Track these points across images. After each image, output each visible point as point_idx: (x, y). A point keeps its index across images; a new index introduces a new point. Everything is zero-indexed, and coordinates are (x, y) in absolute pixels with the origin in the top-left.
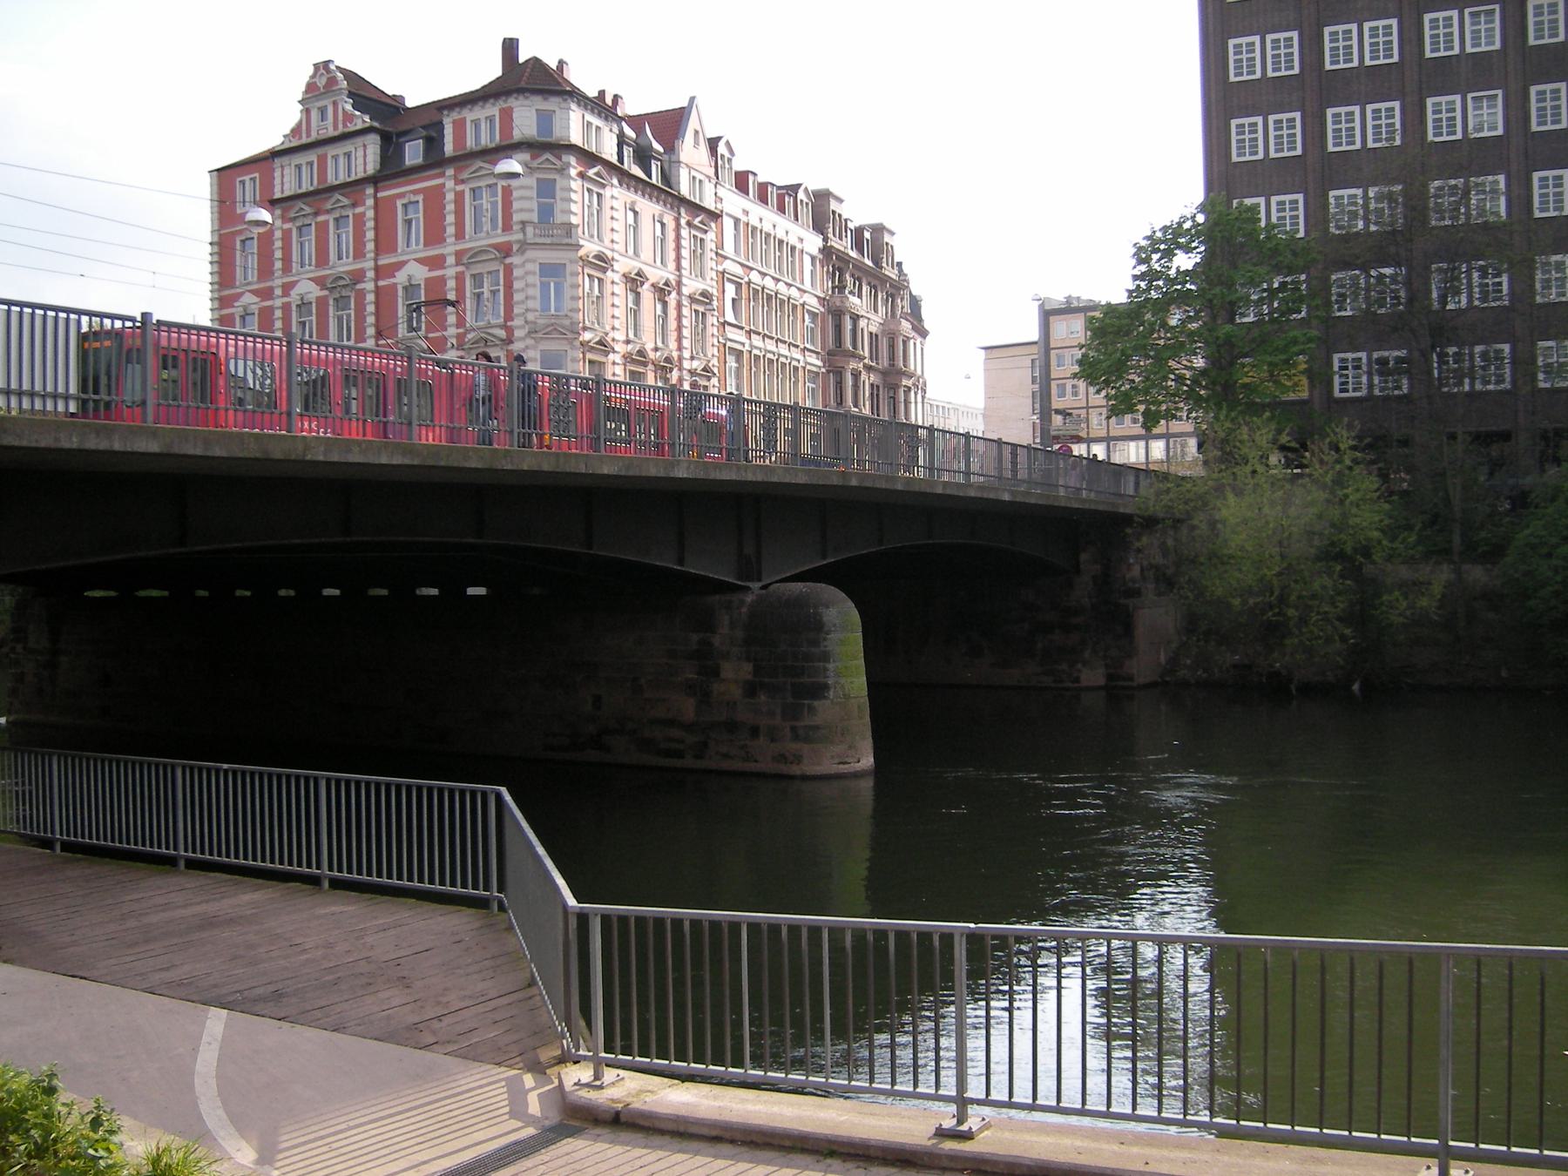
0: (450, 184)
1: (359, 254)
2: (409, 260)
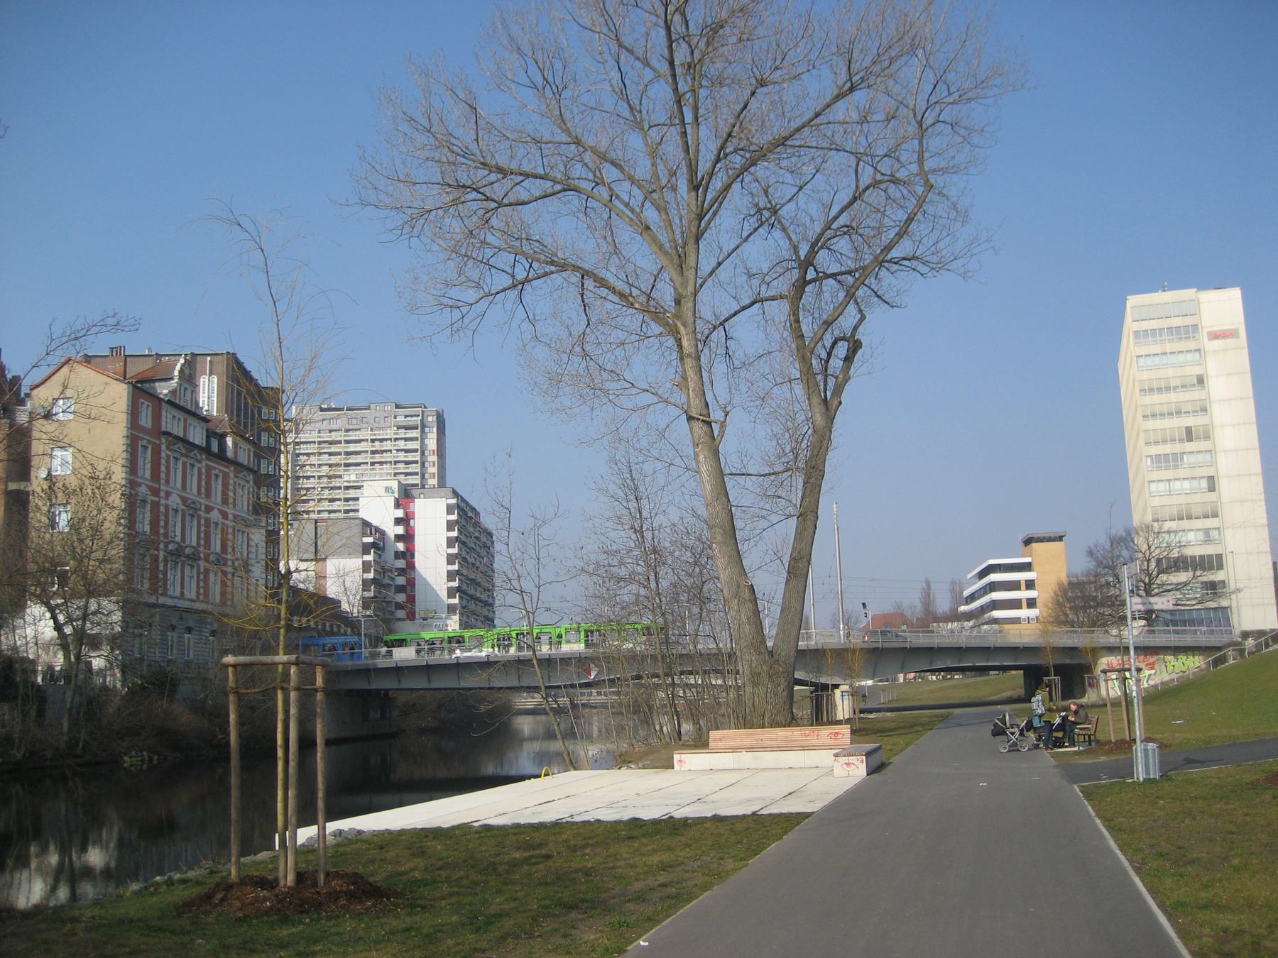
0: (232, 475)
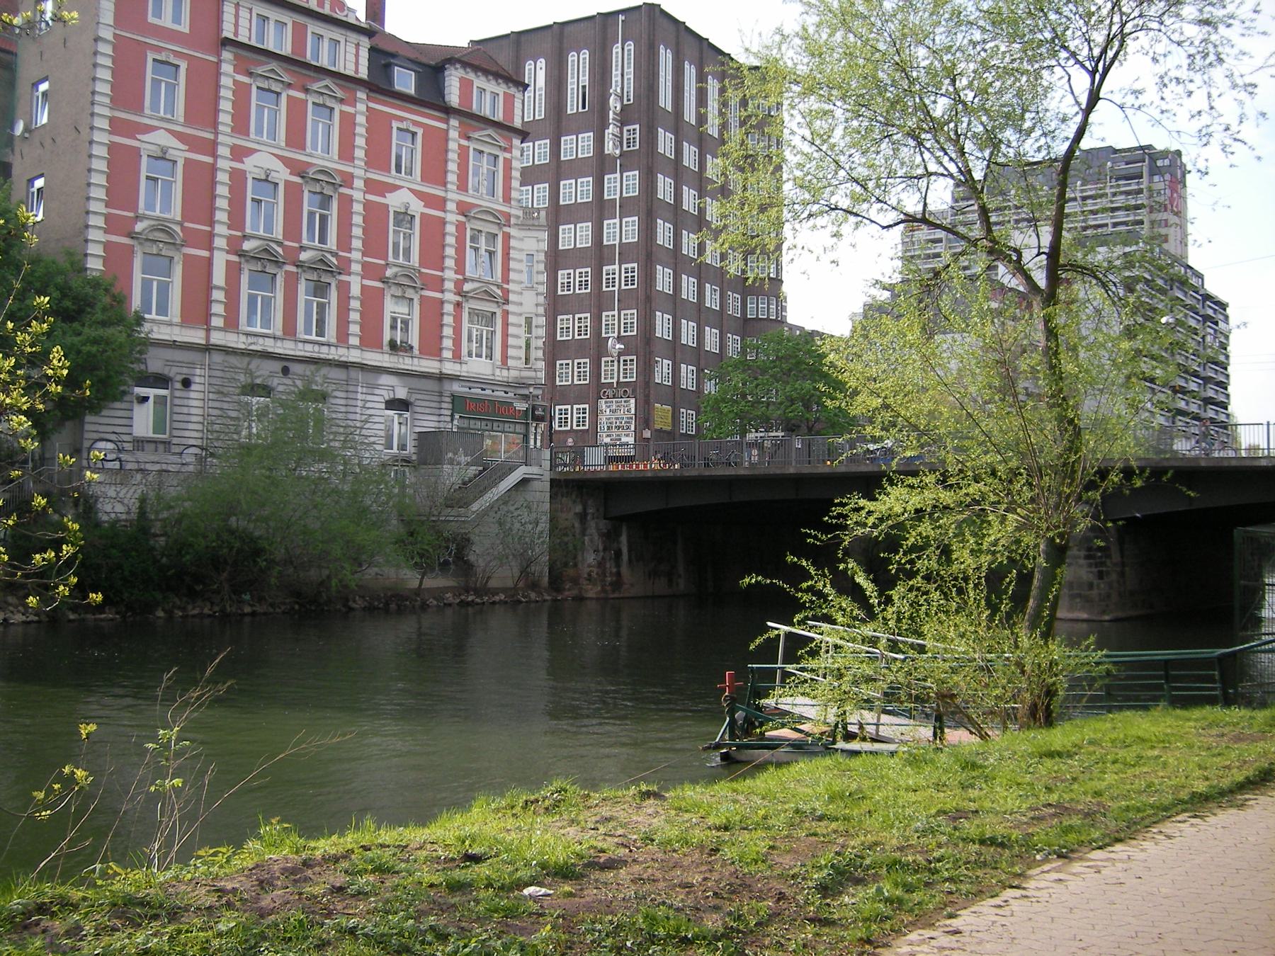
0: (453, 134)
1: (346, 153)
2: (400, 187)
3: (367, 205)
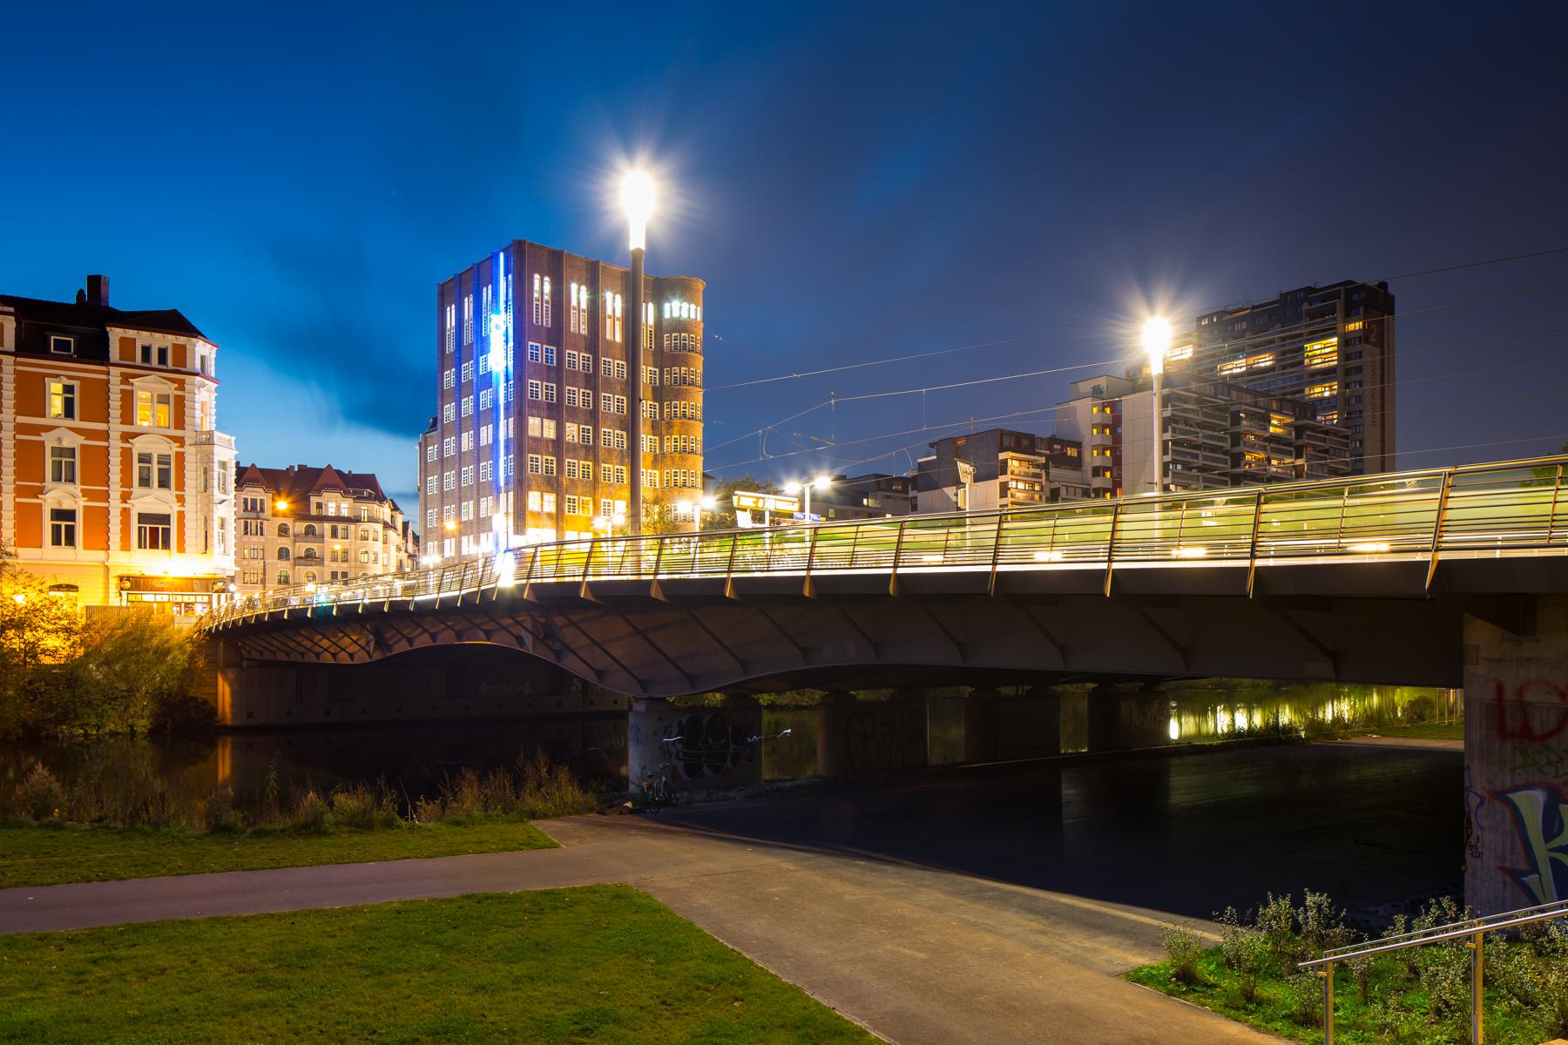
3: (107, 483)
